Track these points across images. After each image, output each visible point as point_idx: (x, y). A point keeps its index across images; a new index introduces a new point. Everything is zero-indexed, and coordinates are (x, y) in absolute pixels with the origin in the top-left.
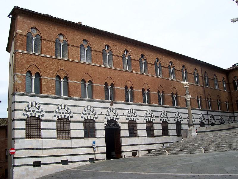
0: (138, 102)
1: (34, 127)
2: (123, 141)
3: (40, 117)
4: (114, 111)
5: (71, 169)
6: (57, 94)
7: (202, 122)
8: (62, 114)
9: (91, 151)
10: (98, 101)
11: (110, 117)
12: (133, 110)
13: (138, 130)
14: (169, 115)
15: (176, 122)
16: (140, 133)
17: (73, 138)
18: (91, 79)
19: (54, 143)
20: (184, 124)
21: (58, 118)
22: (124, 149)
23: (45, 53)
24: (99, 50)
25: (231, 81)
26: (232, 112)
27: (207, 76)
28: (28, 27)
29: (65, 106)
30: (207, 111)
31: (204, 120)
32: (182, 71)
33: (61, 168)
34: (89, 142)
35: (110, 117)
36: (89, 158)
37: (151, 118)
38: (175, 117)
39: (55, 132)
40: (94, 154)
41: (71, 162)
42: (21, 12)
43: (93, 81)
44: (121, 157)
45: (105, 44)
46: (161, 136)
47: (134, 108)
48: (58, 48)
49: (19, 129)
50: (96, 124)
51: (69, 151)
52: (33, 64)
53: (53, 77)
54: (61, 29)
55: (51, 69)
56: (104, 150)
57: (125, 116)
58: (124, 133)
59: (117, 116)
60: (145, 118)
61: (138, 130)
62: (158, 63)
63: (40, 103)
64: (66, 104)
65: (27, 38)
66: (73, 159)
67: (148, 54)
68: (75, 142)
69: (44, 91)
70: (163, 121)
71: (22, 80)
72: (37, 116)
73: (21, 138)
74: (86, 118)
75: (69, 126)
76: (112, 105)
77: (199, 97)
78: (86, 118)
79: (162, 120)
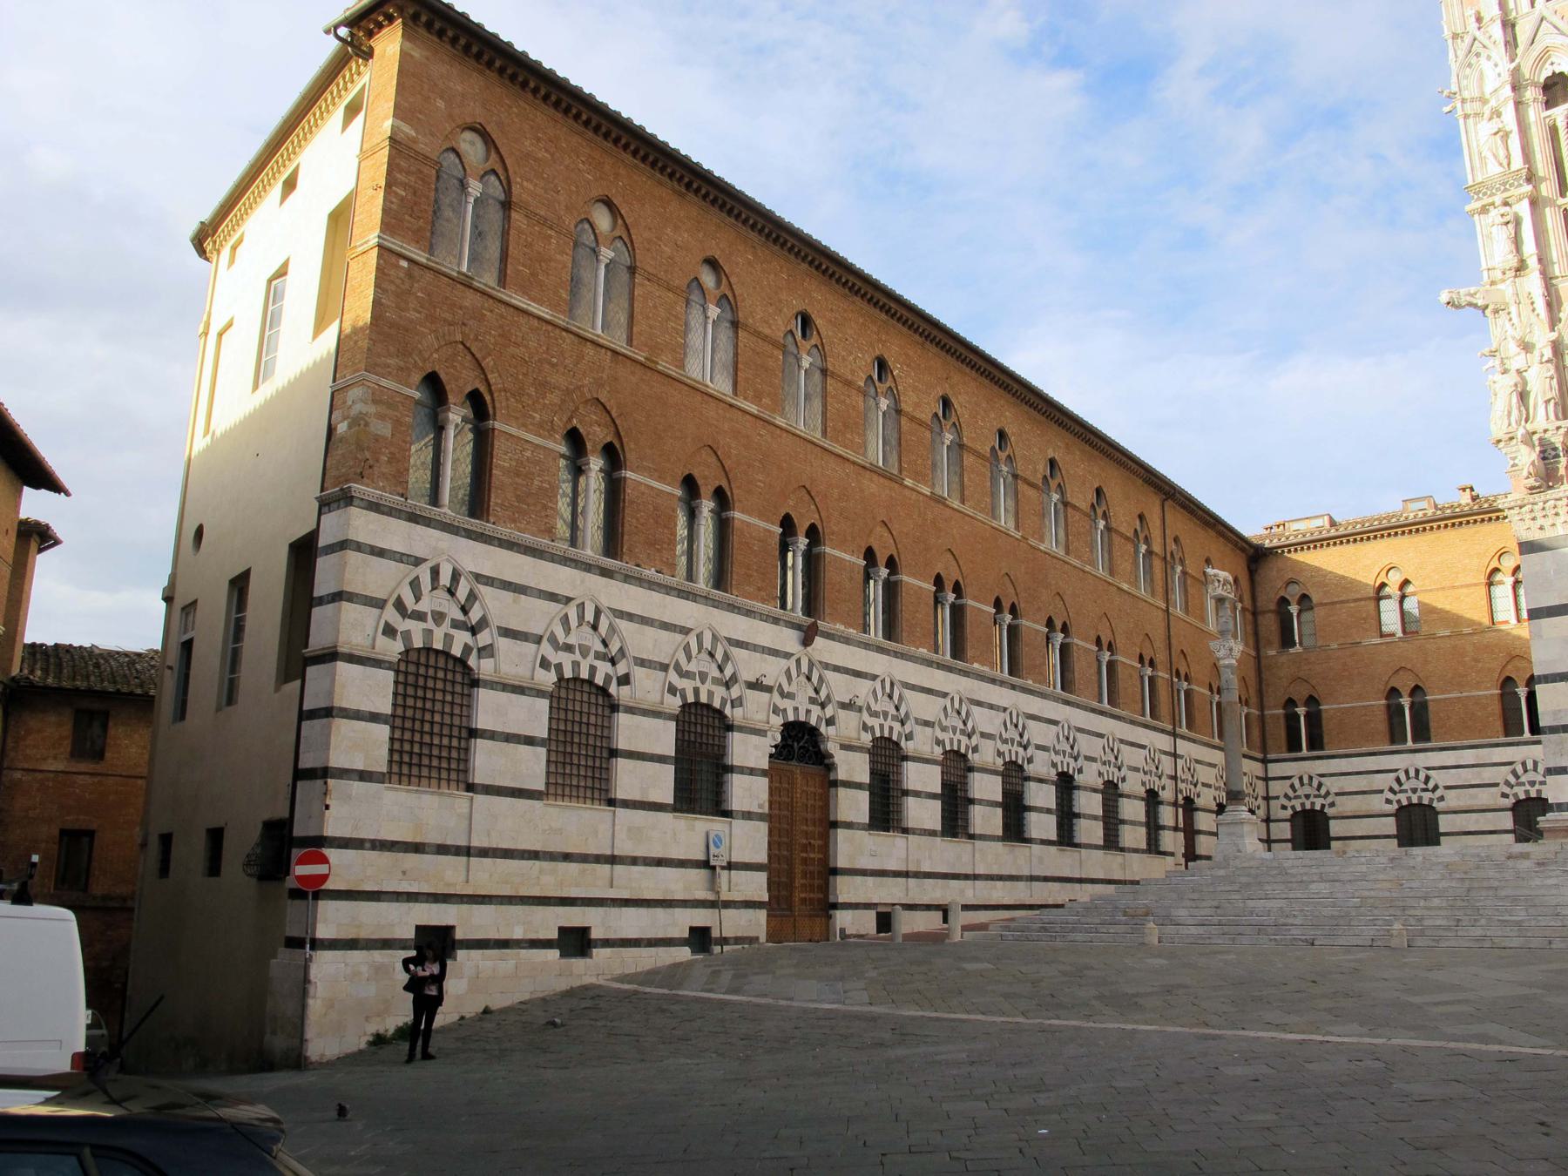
1: (434, 716)
2: (346, 811)
3: (472, 662)
4: (815, 679)
5: (602, 982)
7: (1011, 762)
9: (690, 883)
11: (796, 709)
14: (920, 706)
15: (875, 740)
16: (628, 779)
18: (724, 484)
20: (1086, 789)
21: (561, 679)
22: (845, 889)
23: (525, 291)
25: (1268, 601)
26: (1260, 756)
28: (450, 116)
29: (456, 576)
30: (1174, 735)
33: (553, 973)
34: (686, 834)
35: (796, 709)
37: (714, 688)
38: (869, 708)
40: (712, 904)
41: (607, 943)
42: (424, 18)
43: (736, 493)
44: (826, 935)
45: (798, 305)
46: (1096, 847)
47: (898, 677)
48: (586, 275)
49: (357, 715)
56: (755, 886)
57: (860, 710)
59: (474, 631)
60: (941, 735)
61: (764, 773)
63: (478, 577)
64: (605, 602)
67: (968, 394)
68: (629, 829)
71: (397, 423)
73: (364, 776)
74: (568, 674)
76: (807, 642)
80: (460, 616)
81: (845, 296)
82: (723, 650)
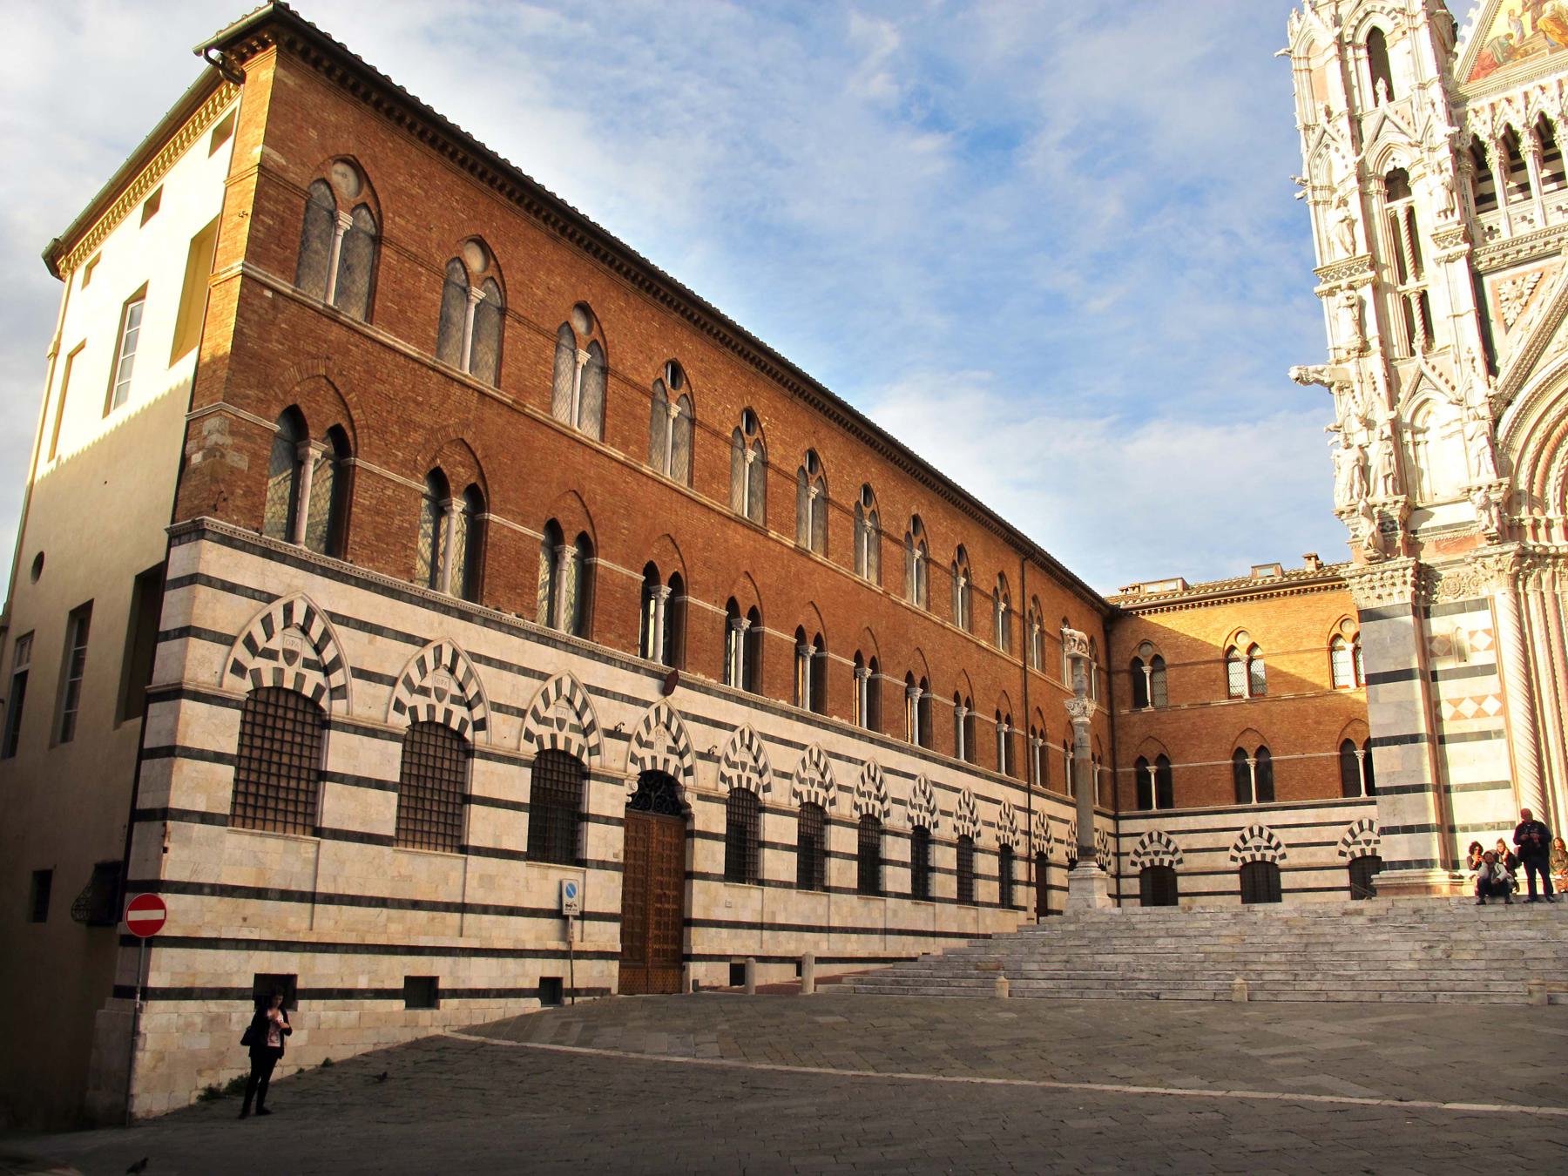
0: (771, 694)
1: (281, 763)
5: (448, 1033)
6: (1141, 807)
8: (281, 663)
9: (542, 933)
10: (609, 660)
11: (654, 758)
12: (751, 735)
13: (619, 822)
15: (732, 790)
16: (482, 826)
17: (480, 851)
18: (589, 530)
19: (380, 866)
22: (701, 941)
23: (391, 327)
24: (637, 379)
25: (1122, 661)
26: (1111, 812)
27: (1040, 620)
30: (1029, 791)
31: (932, 813)
32: (803, 483)
33: (395, 1023)
34: (539, 883)
35: (654, 758)
36: (407, 978)
37: (572, 735)
38: (727, 759)
39: (388, 801)
42: (299, 46)
49: (201, 755)
50: (335, 738)
51: (445, 929)
52: (322, 371)
53: (413, 476)
54: (647, 313)
55: (408, 424)
57: (718, 760)
58: (710, 856)
62: (867, 511)
63: (334, 617)
64: (463, 646)
65: (307, 208)
66: (462, 974)
67: (834, 450)
69: (360, 544)
70: (548, 746)
71: (254, 456)
72: (308, 691)
75: (462, 775)
76: (666, 691)
77: (810, 639)
78: (423, 717)
79: (540, 744)
80: (312, 656)
81: (716, 347)
82: (581, 697)
